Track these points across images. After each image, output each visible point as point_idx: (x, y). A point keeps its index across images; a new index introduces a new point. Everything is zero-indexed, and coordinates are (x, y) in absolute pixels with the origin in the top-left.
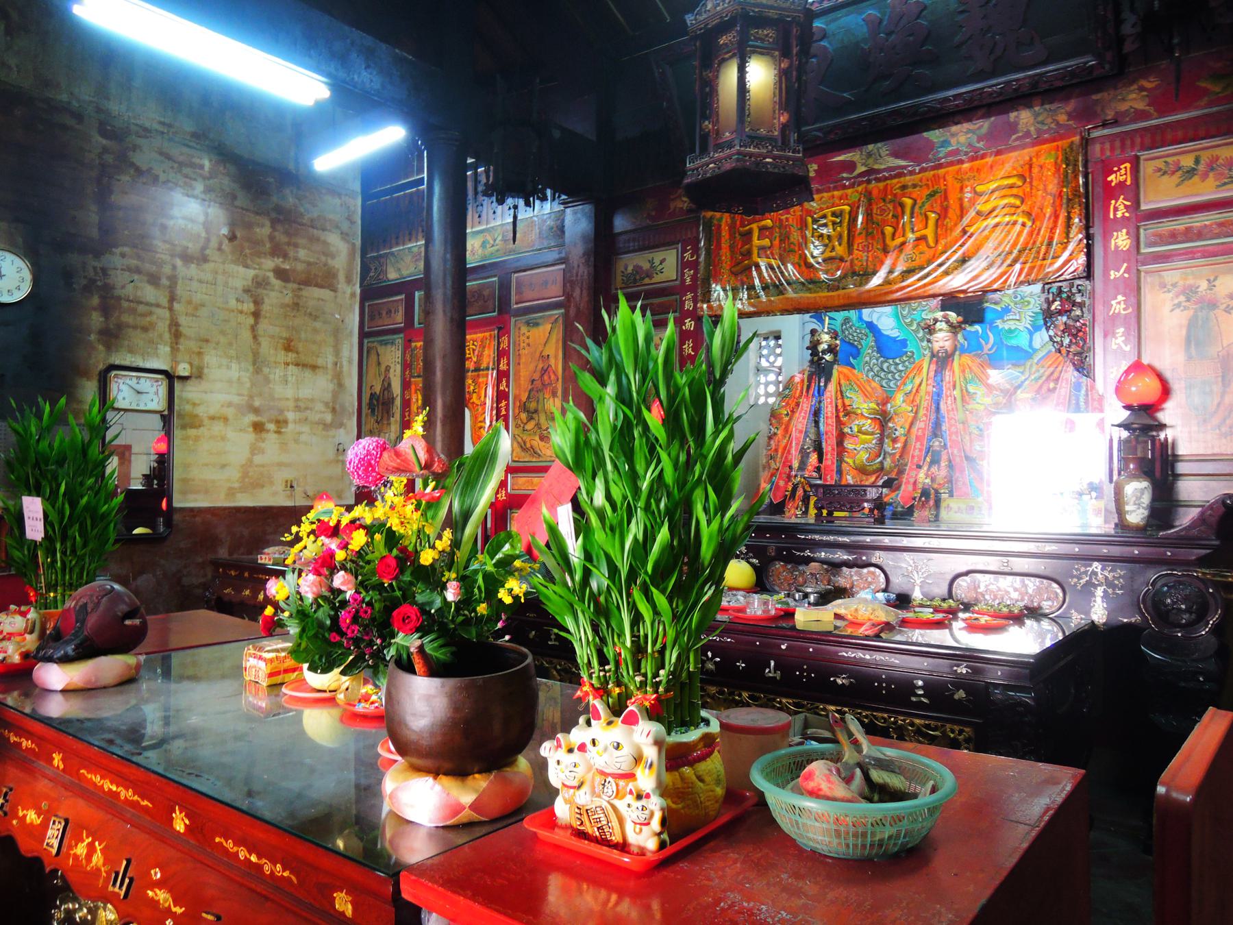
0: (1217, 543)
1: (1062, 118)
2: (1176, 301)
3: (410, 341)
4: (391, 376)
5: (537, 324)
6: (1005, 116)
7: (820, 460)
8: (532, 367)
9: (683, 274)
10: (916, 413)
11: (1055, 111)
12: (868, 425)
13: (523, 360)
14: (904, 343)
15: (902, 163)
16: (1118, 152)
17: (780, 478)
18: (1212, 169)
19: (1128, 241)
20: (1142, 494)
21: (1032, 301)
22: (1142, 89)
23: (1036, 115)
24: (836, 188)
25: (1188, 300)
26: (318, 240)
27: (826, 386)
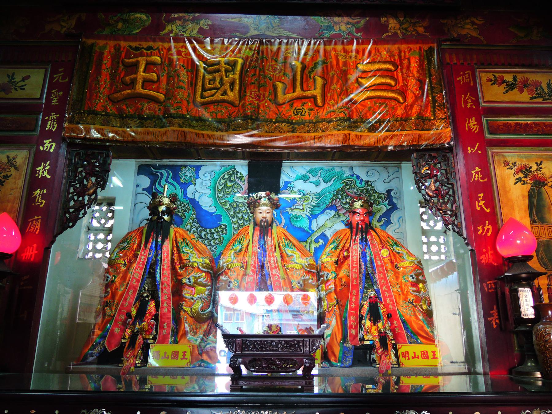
1: (421, 30)
2: (517, 177)
7: (157, 307)
11: (415, 23)
12: (203, 278)
14: (219, 217)
17: (116, 325)
18: (525, 86)
21: (311, 198)
23: (401, 24)
25: (526, 177)
27: (163, 242)
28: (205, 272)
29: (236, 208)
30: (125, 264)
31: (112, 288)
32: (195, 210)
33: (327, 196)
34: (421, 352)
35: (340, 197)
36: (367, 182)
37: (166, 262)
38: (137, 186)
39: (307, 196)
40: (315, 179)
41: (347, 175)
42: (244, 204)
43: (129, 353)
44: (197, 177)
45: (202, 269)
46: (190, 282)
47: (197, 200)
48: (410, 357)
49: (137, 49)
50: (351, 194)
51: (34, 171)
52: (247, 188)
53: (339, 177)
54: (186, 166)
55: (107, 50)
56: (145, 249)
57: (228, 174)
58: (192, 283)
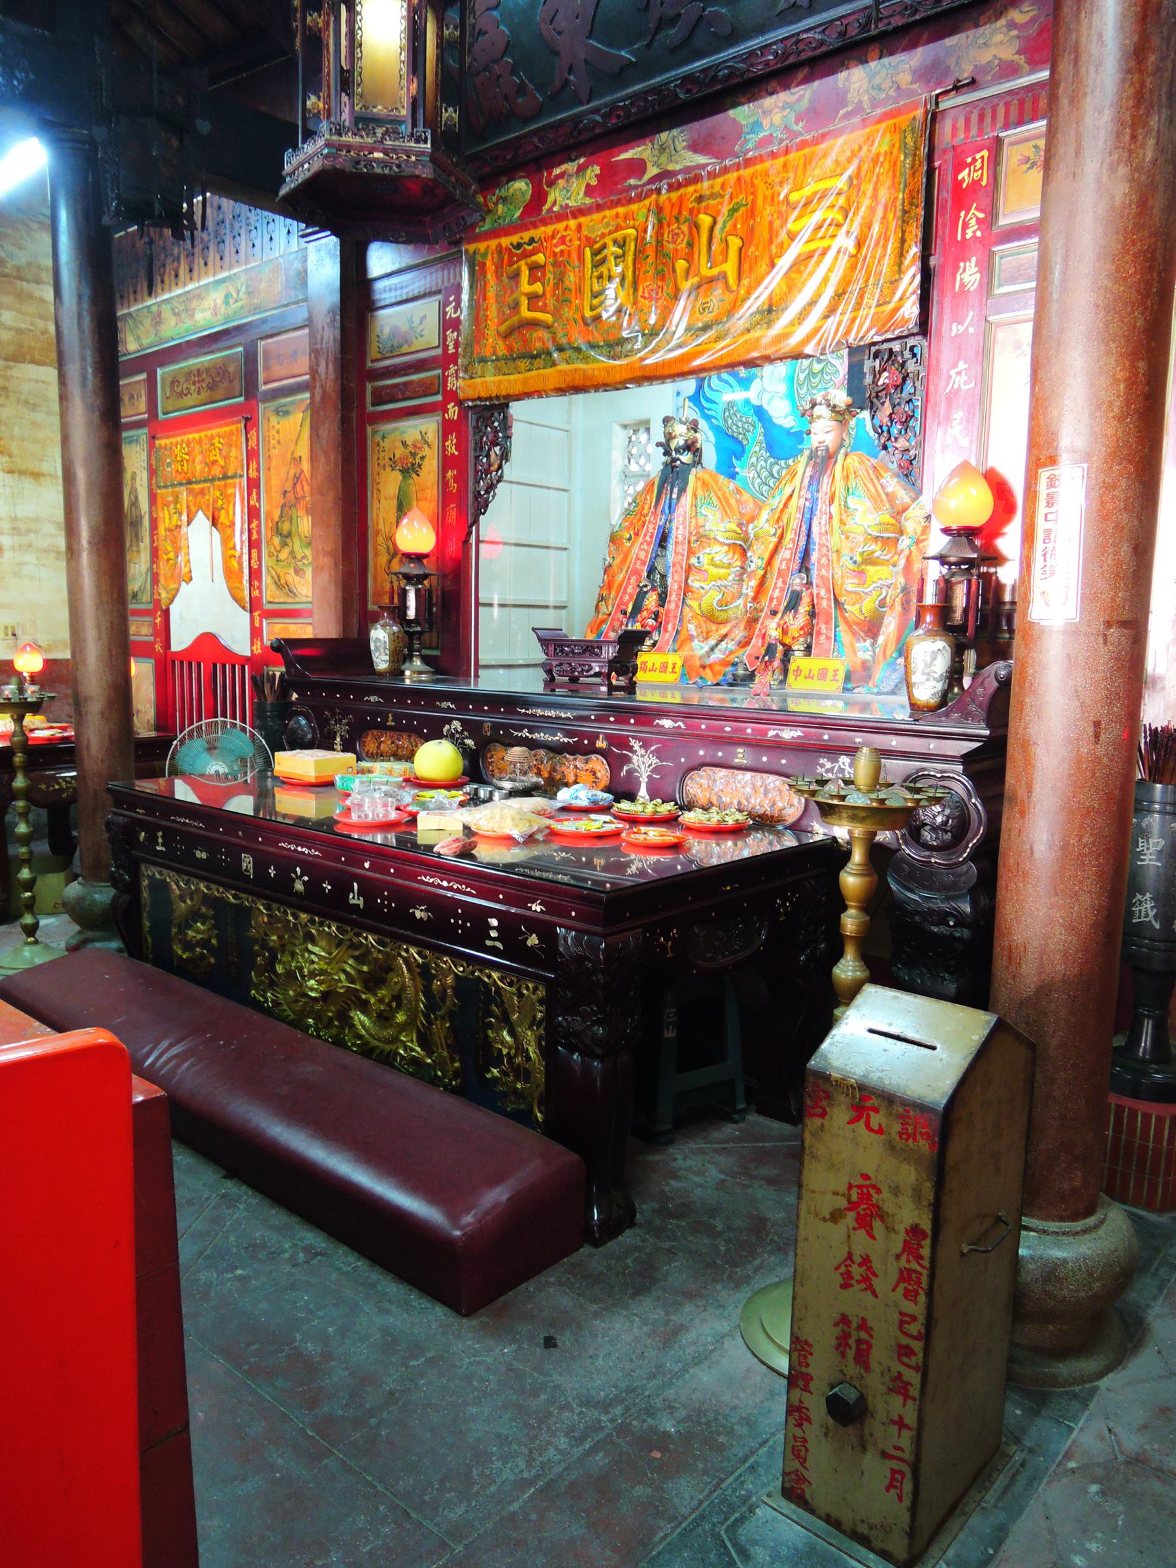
0: (987, 732)
3: (154, 438)
4: (138, 485)
5: (287, 413)
6: (831, 79)
8: (283, 474)
9: (445, 337)
10: (781, 537)
12: (720, 553)
13: (273, 464)
15: (701, 159)
16: (974, 131)
19: (978, 276)
20: (934, 658)
22: (1012, 25)
24: (618, 203)
26: (30, 296)
30: (629, 539)
32: (764, 427)
38: (678, 394)
47: (765, 407)
49: (519, 246)
51: (444, 449)
55: (489, 257)
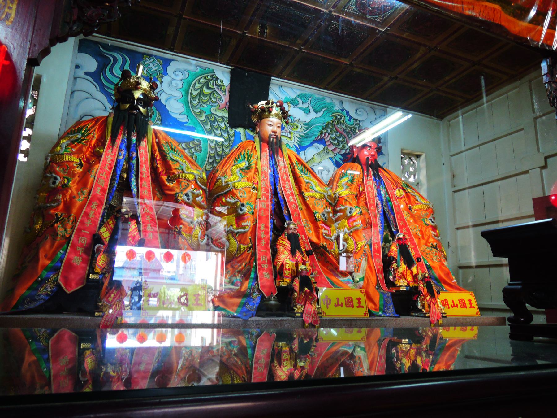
28: (202, 189)
29: (214, 122)
30: (80, 164)
31: (64, 195)
32: (160, 115)
33: (316, 127)
34: (345, 298)
35: (329, 131)
36: (356, 120)
37: (144, 170)
38: (77, 67)
39: (296, 123)
40: (305, 106)
41: (337, 109)
42: (223, 119)
43: (112, 295)
44: (165, 73)
45: (200, 185)
46: (188, 199)
48: (450, 306)
50: (340, 130)
52: (228, 100)
53: (329, 109)
54: (150, 56)
56: (113, 146)
57: (205, 78)
58: (190, 201)
